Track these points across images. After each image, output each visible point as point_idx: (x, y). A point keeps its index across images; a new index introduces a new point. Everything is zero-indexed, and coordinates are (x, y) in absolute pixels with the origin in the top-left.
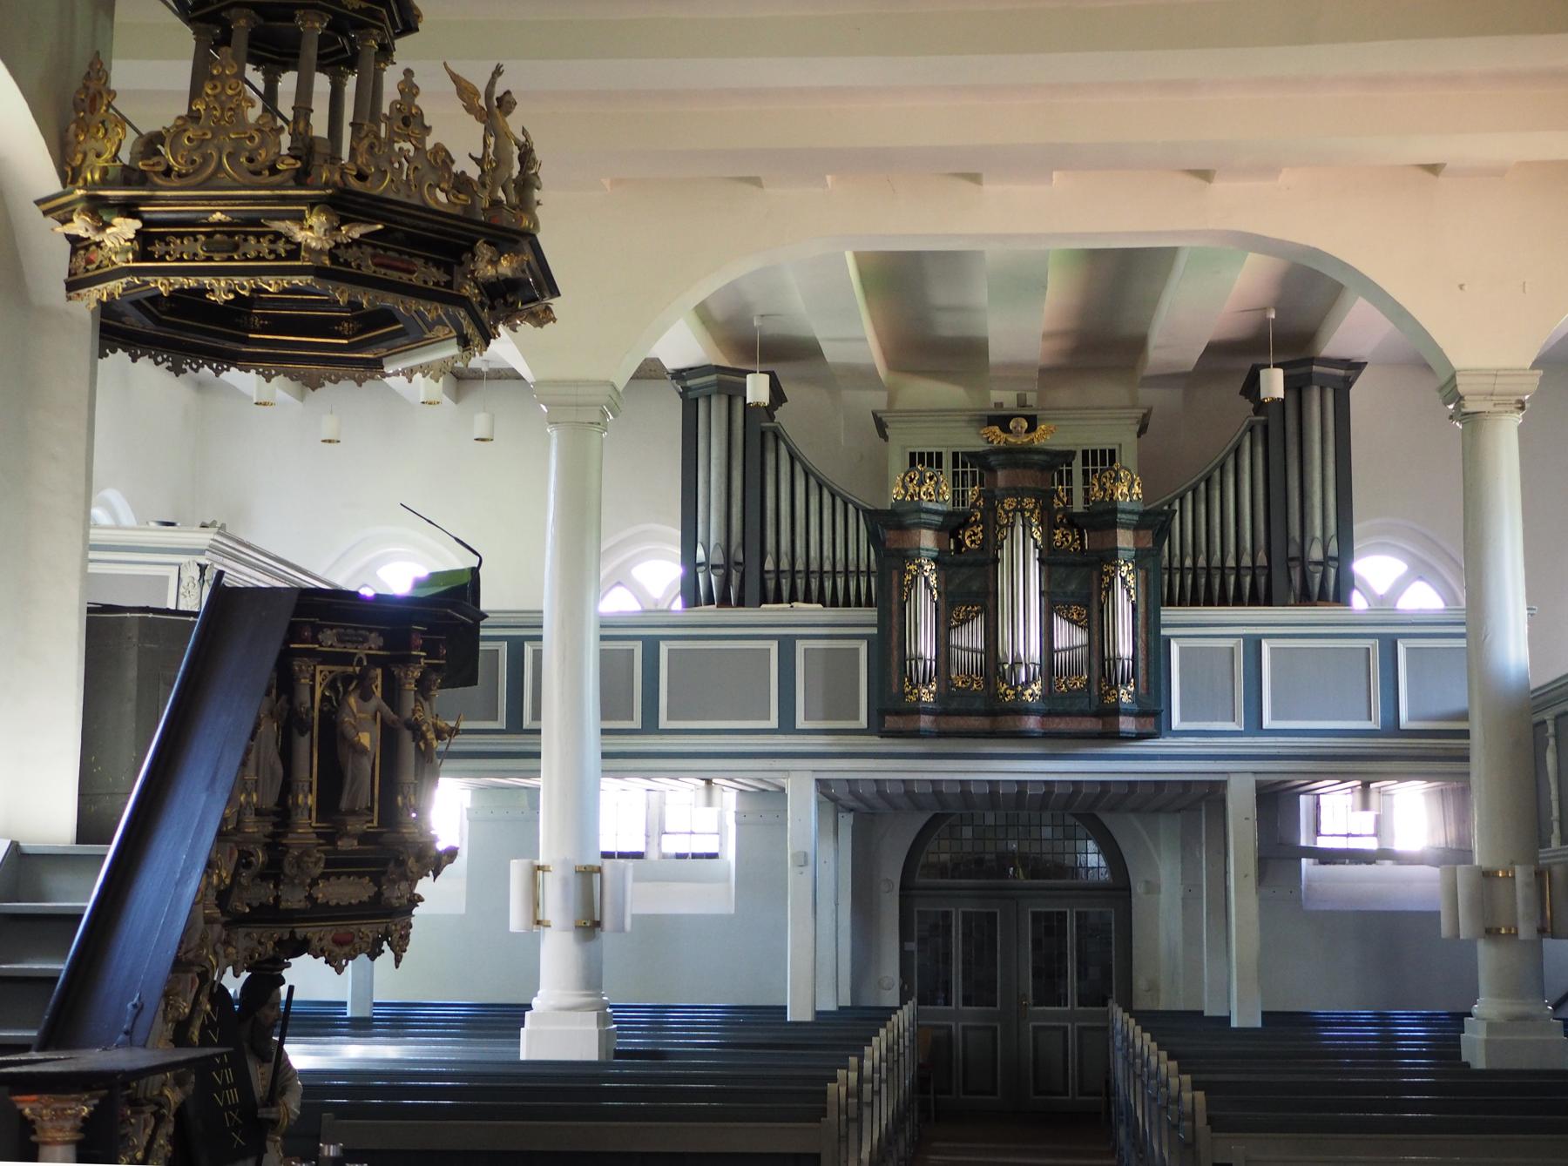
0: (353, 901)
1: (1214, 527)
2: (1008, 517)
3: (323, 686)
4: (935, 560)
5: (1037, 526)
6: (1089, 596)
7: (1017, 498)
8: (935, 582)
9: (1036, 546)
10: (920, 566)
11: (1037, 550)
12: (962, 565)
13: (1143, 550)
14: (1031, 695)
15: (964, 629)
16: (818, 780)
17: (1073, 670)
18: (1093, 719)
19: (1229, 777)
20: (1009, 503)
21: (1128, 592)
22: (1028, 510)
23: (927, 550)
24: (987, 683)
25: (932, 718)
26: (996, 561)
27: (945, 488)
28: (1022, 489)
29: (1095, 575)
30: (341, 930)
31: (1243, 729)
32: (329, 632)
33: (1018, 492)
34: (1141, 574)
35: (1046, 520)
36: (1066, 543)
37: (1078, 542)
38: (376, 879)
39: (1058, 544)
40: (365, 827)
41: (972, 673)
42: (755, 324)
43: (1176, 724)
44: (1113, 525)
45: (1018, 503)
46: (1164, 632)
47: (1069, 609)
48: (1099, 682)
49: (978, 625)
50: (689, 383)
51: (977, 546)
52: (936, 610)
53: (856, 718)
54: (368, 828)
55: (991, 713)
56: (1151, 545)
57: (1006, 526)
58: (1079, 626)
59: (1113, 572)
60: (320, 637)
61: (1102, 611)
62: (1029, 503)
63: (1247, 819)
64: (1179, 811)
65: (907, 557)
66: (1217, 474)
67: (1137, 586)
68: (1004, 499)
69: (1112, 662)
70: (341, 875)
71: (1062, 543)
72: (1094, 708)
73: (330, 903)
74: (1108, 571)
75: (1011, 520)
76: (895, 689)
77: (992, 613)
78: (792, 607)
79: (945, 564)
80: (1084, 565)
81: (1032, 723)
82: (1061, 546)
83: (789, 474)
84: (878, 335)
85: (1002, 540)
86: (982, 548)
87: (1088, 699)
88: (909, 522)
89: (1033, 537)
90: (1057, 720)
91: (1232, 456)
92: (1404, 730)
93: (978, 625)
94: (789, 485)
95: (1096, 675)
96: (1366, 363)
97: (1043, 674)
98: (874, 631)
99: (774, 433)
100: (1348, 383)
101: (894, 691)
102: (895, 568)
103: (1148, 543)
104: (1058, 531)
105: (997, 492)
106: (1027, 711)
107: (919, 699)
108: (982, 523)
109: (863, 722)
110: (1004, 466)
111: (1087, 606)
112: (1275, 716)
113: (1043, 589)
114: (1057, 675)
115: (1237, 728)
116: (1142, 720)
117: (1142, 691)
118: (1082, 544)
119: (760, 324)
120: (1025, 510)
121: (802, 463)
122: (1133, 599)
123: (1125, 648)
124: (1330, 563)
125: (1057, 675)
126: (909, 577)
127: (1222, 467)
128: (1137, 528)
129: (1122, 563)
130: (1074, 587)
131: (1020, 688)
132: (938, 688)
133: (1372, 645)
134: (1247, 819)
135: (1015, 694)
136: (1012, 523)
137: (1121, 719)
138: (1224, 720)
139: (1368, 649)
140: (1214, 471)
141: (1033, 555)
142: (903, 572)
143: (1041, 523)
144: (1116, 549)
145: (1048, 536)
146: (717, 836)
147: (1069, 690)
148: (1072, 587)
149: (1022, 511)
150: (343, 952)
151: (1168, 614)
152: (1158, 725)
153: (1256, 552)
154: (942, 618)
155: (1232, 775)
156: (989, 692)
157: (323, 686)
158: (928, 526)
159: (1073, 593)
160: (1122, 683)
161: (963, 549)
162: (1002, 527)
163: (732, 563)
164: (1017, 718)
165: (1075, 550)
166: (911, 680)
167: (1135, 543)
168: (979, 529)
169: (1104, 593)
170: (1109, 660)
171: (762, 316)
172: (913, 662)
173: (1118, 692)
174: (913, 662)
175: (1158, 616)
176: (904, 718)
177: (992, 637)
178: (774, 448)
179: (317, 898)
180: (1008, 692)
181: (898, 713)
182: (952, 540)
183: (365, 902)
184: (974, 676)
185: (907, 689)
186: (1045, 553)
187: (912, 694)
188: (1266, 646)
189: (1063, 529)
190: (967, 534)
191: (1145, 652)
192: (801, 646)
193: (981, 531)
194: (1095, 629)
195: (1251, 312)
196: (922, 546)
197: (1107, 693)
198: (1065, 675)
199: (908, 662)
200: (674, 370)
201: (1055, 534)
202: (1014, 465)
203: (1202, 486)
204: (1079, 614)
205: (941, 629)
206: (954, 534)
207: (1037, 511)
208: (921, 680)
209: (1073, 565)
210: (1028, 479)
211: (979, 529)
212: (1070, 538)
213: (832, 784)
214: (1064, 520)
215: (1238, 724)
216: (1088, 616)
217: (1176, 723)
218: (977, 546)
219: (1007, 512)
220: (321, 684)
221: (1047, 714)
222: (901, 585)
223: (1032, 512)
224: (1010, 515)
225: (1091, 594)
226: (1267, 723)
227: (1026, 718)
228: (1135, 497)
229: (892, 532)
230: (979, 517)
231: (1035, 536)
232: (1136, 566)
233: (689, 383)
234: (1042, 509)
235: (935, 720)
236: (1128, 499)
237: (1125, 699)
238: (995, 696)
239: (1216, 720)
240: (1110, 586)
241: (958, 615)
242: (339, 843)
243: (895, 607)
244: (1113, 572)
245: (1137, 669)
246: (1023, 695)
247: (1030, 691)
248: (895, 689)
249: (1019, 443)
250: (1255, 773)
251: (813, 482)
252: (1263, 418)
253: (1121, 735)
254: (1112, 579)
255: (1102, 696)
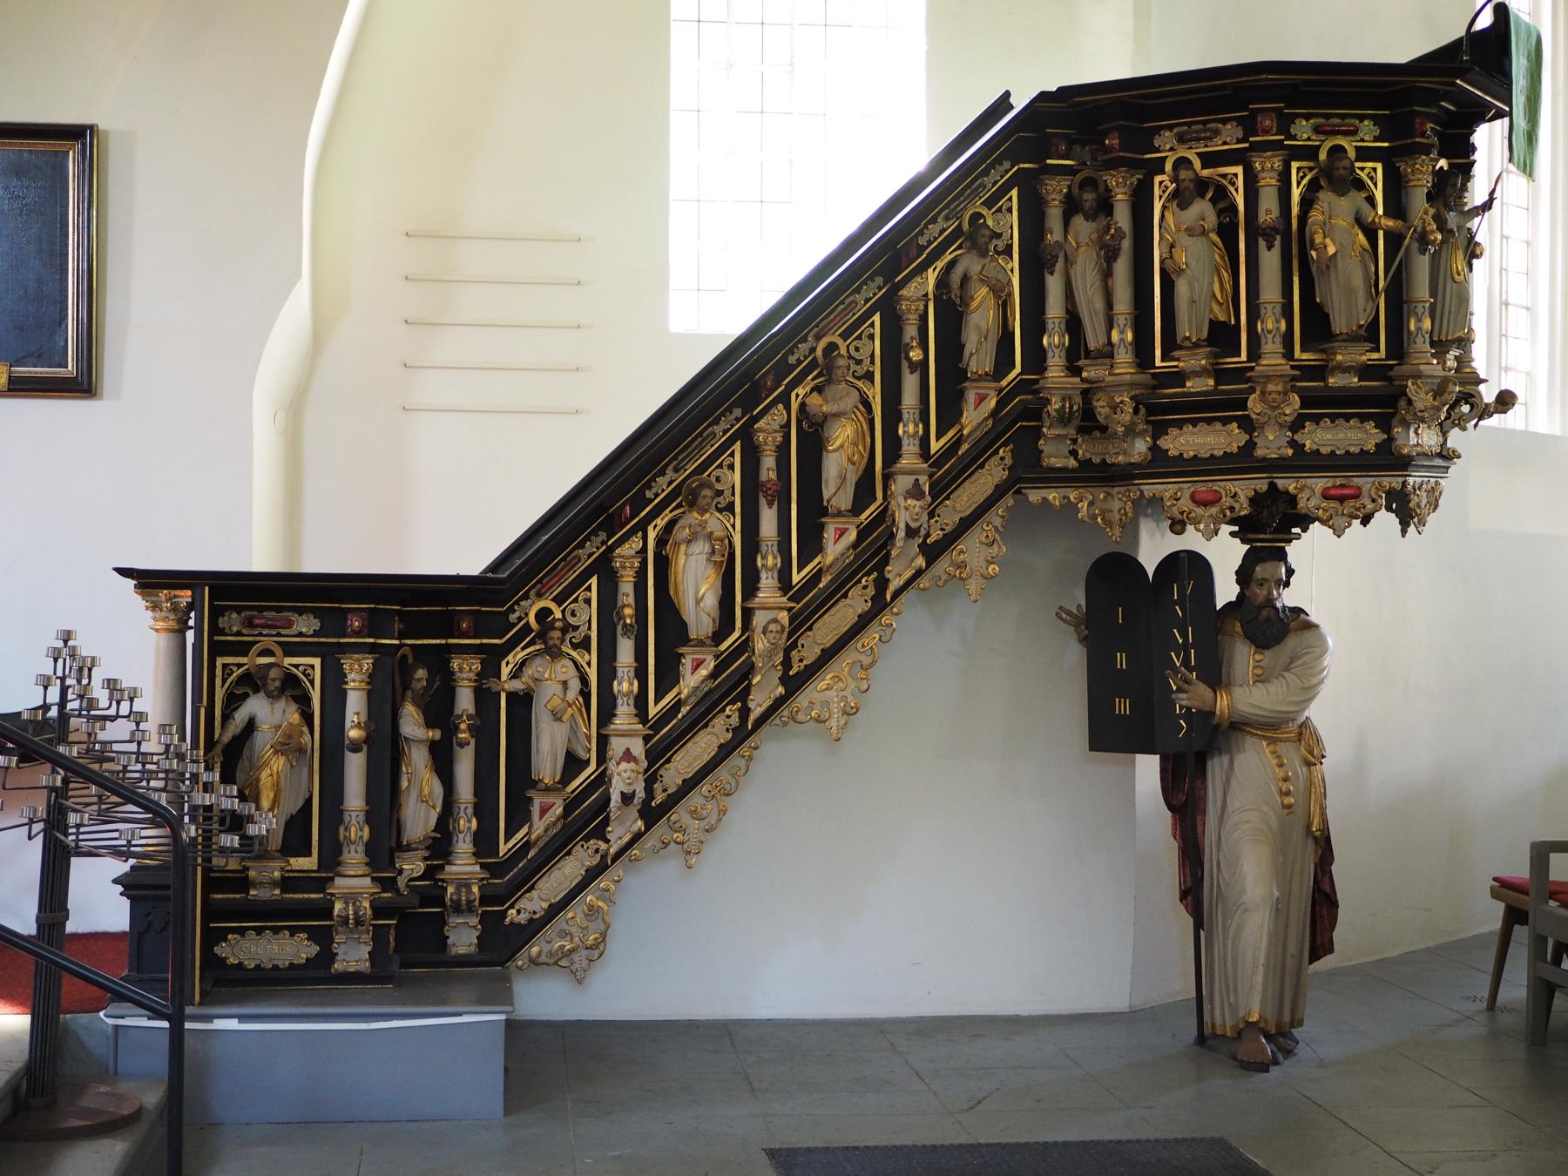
0: (1216, 452)
3: (1163, 199)
30: (1201, 488)
32: (1167, 134)
38: (1385, 424)
40: (1364, 358)
54: (1369, 360)
60: (1293, 131)
70: (1197, 423)
73: (1185, 456)
92: (1502, 901)
146: (1524, 406)
150: (1206, 514)
157: (1163, 199)
179: (1304, 445)
183: (1368, 452)
220: (1161, 197)
242: (1330, 381)
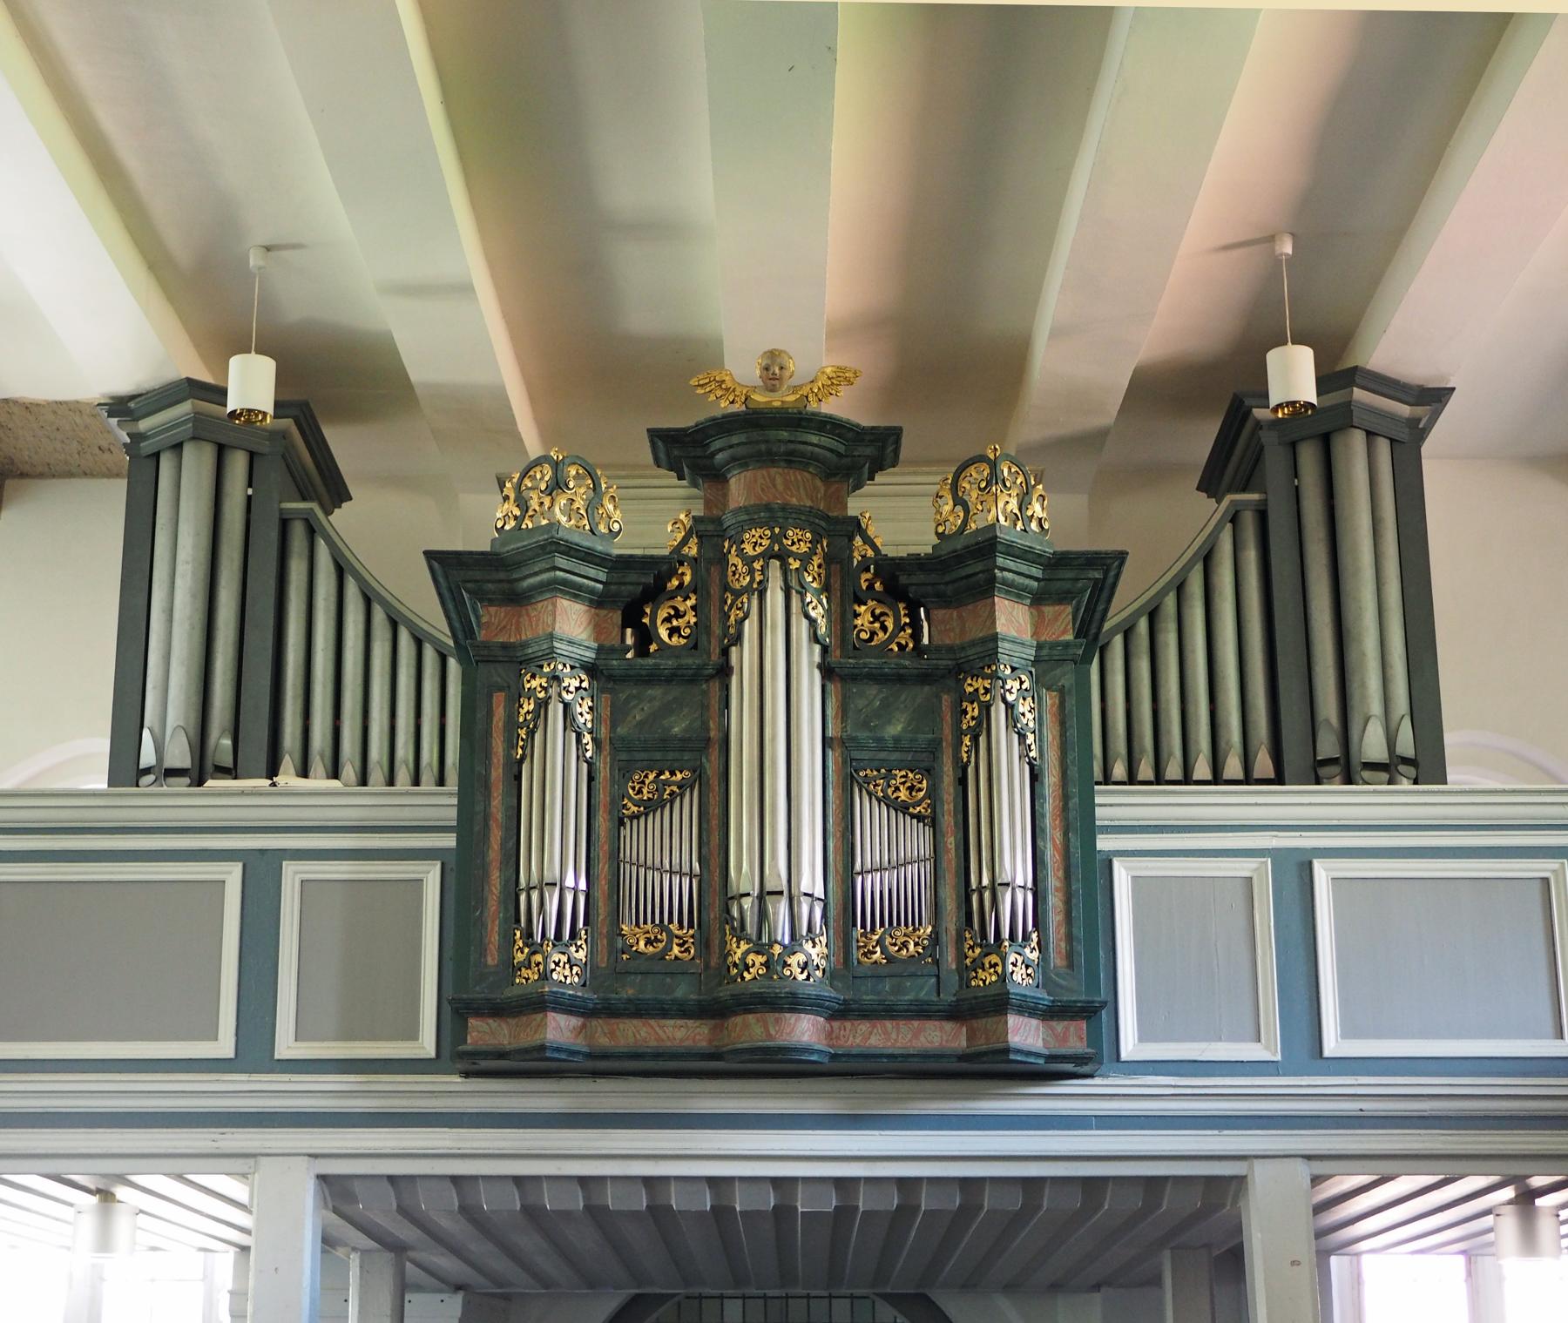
1: (1167, 701)
2: (751, 572)
4: (591, 670)
5: (818, 593)
6: (934, 749)
7: (772, 529)
8: (589, 717)
9: (815, 638)
10: (555, 678)
11: (817, 648)
12: (651, 678)
13: (1054, 645)
14: (804, 967)
15: (653, 822)
16: (322, 1178)
17: (894, 916)
18: (948, 1026)
19: (1251, 1168)
20: (755, 540)
21: (1022, 737)
22: (796, 556)
23: (571, 642)
24: (704, 943)
25: (575, 1021)
26: (724, 671)
27: (611, 507)
28: (784, 508)
29: (946, 700)
31: (1278, 1057)
33: (771, 515)
34: (1050, 699)
35: (836, 584)
36: (881, 634)
37: (909, 631)
39: (864, 636)
41: (671, 921)
42: (252, 263)
43: (1130, 1047)
44: (984, 589)
45: (774, 539)
46: (1104, 843)
47: (889, 776)
48: (960, 939)
49: (686, 811)
50: (144, 425)
51: (683, 641)
52: (591, 779)
53: (412, 1034)
55: (714, 1010)
56: (1069, 637)
57: (748, 590)
58: (913, 816)
59: (987, 691)
61: (962, 782)
62: (798, 540)
63: (1295, 1263)
64: (1097, 1287)
65: (528, 661)
66: (1170, 602)
67: (1040, 725)
68: (744, 531)
69: (987, 895)
71: (873, 634)
72: (948, 997)
74: (977, 690)
75: (758, 578)
76: (492, 960)
77: (715, 783)
78: (274, 785)
79: (611, 678)
80: (925, 678)
81: (805, 1030)
82: (871, 639)
83: (333, 599)
84: (506, 315)
85: (740, 622)
86: (694, 646)
87: (933, 980)
88: (526, 583)
89: (807, 616)
90: (864, 1026)
91: (1199, 567)
93: (686, 811)
94: (332, 624)
95: (951, 922)
96: (1454, 389)
97: (831, 923)
98: (449, 841)
99: (307, 521)
100: (1418, 432)
101: (490, 961)
102: (501, 689)
103: (1064, 632)
104: (863, 608)
105: (729, 520)
106: (795, 1003)
107: (545, 976)
108: (695, 592)
109: (426, 1045)
110: (742, 462)
111: (929, 772)
112: (1349, 1030)
113: (830, 733)
114: (863, 926)
115: (1266, 1056)
116: (1059, 1026)
117: (1057, 960)
118: (916, 636)
119: (261, 263)
120: (791, 554)
121: (331, 544)
122: (1032, 754)
123: (1016, 866)
124: (1402, 768)
125: (863, 926)
126: (528, 706)
127: (1180, 588)
128: (1038, 600)
129: (1008, 671)
130: (899, 728)
131: (777, 949)
132: (591, 954)
133: (1554, 871)
134: (1295, 1263)
135: (766, 965)
136: (760, 582)
137: (1013, 1020)
138: (1235, 1038)
139: (1546, 881)
140: (1167, 594)
141: (808, 658)
142: (517, 694)
143: (826, 588)
144: (995, 638)
145: (842, 620)
147: (890, 959)
148: (895, 729)
149: (783, 557)
151: (1112, 805)
152: (1094, 1038)
153: (1251, 755)
154: (602, 797)
155: (1259, 1166)
156: (707, 966)
158: (575, 592)
159: (897, 739)
160: (1012, 937)
161: (653, 648)
162: (737, 594)
163: (209, 767)
164: (771, 1017)
165: (902, 647)
166: (529, 934)
167: (1035, 634)
168: (689, 603)
169: (967, 741)
170: (981, 889)
171: (268, 249)
172: (535, 896)
173: (1004, 959)
174: (535, 896)
175: (1089, 807)
176: (512, 1021)
177: (715, 839)
178: (306, 552)
180: (750, 958)
181: (498, 1010)
182: (629, 631)
184: (674, 927)
185: (520, 957)
186: (835, 657)
187: (529, 967)
188: (1322, 872)
189: (871, 603)
190: (663, 613)
191: (1061, 874)
192: (293, 875)
193: (693, 608)
194: (948, 820)
195: (1236, 253)
196: (558, 631)
197: (978, 965)
198: (882, 925)
199: (523, 897)
200: (112, 398)
201: (856, 615)
202: (765, 458)
203: (1143, 625)
204: (911, 789)
205: (603, 823)
206: (632, 617)
207: (816, 561)
208: (551, 934)
209: (899, 679)
210: (796, 488)
211: (689, 603)
212: (890, 624)
213: (357, 1187)
214: (878, 586)
215: (1267, 1048)
216: (933, 793)
217: (1130, 1047)
218: (683, 641)
219: (748, 561)
221: (841, 1012)
222: (512, 724)
223: (805, 559)
224: (757, 565)
225: (940, 741)
226: (1333, 1044)
227: (791, 1018)
228: (1034, 525)
229: (492, 610)
230: (687, 579)
231: (813, 614)
232: (1038, 681)
233: (144, 425)
234: (829, 560)
235: (584, 1026)
236: (1020, 526)
237: (1019, 975)
238: (723, 970)
239: (1220, 1039)
240: (979, 724)
241: (640, 792)
243: (497, 773)
244: (987, 691)
245: (1045, 911)
246: (785, 965)
247: (801, 958)
248: (492, 960)
249: (777, 404)
250: (1309, 1157)
251: (379, 616)
252: (1255, 496)
253: (1012, 1057)
254: (986, 708)
255: (966, 971)
